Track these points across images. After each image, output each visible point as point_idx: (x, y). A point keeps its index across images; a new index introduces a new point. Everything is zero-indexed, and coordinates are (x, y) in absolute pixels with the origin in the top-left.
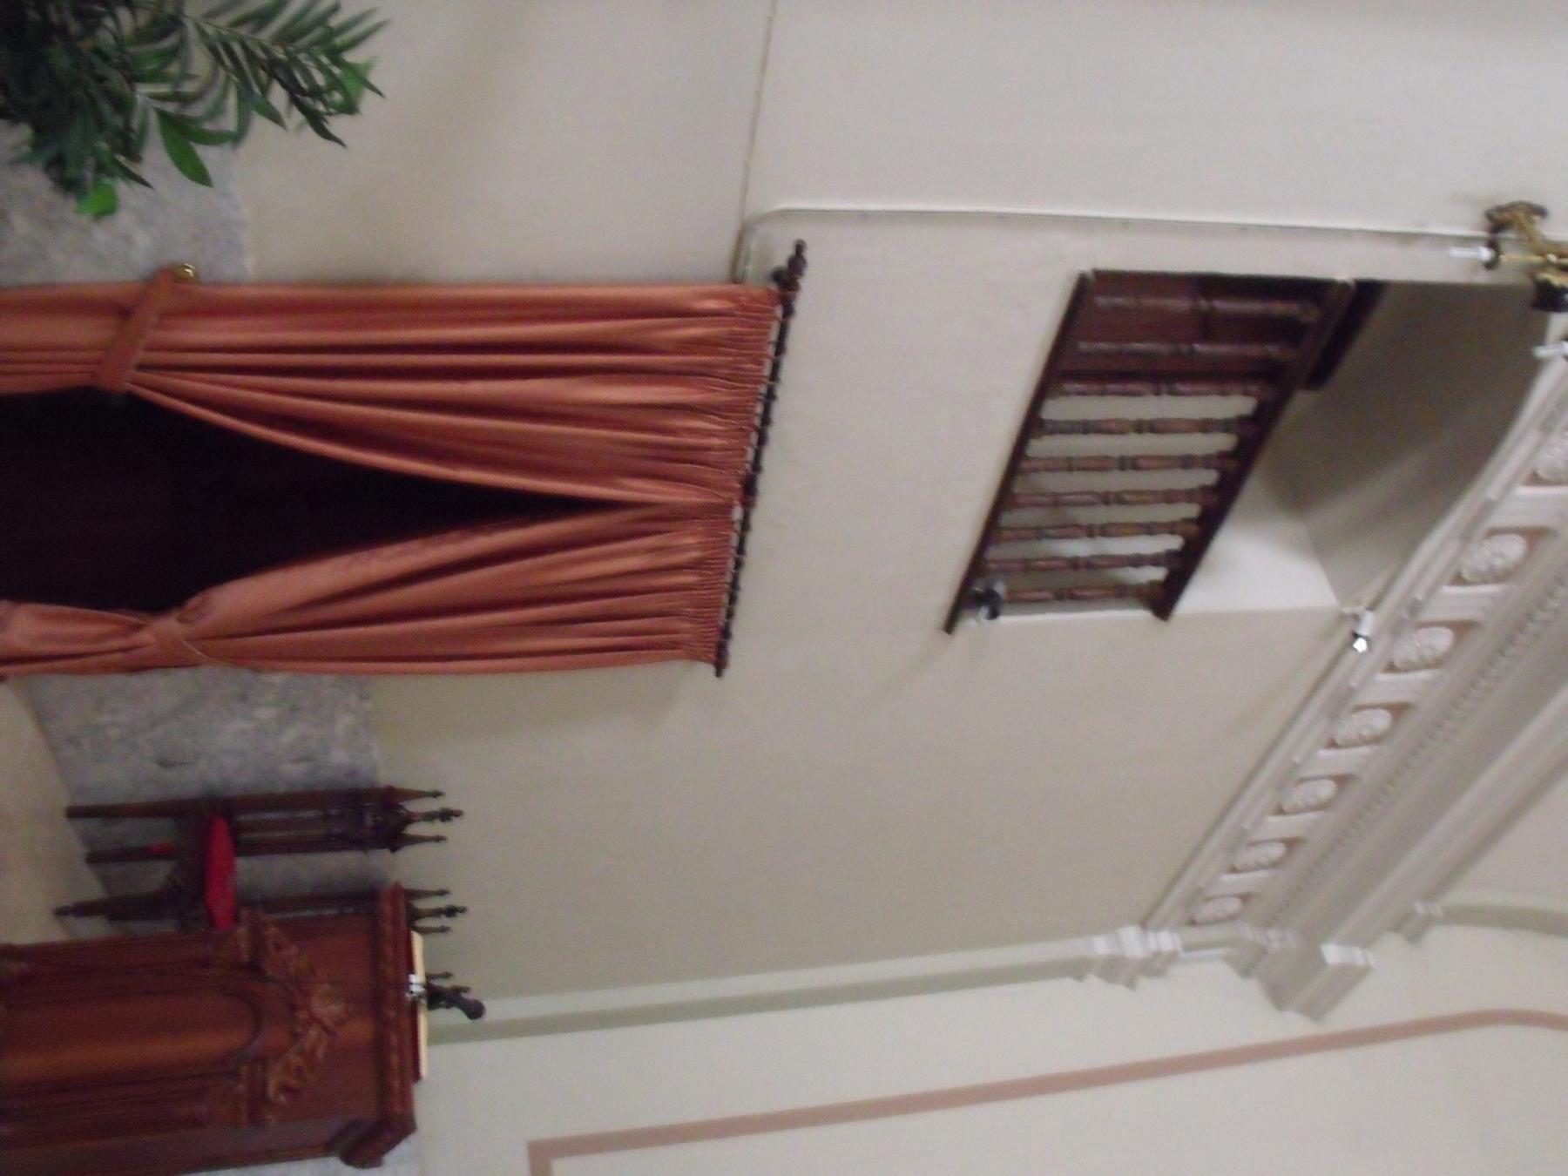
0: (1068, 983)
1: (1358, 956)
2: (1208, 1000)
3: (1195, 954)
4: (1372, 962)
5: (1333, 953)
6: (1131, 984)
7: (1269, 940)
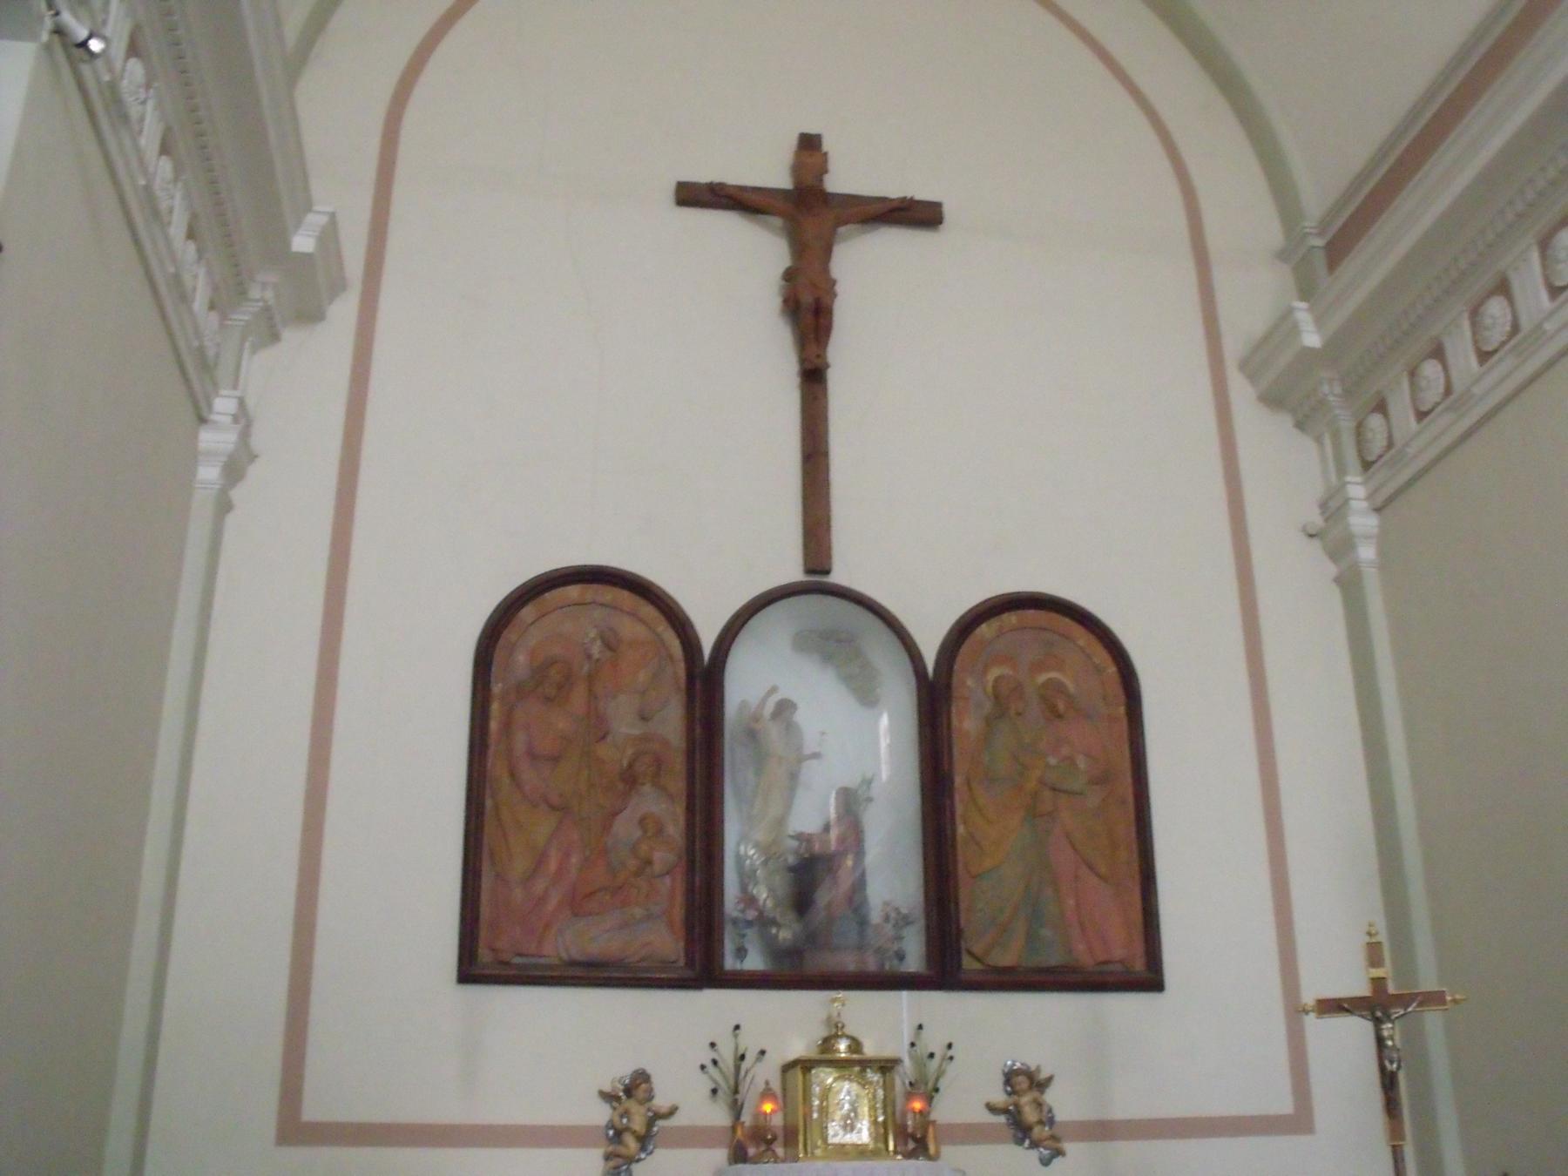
0: (231, 520)
1: (315, 220)
2: (290, 386)
3: (241, 381)
4: (329, 209)
5: (303, 243)
6: (253, 457)
7: (262, 299)
